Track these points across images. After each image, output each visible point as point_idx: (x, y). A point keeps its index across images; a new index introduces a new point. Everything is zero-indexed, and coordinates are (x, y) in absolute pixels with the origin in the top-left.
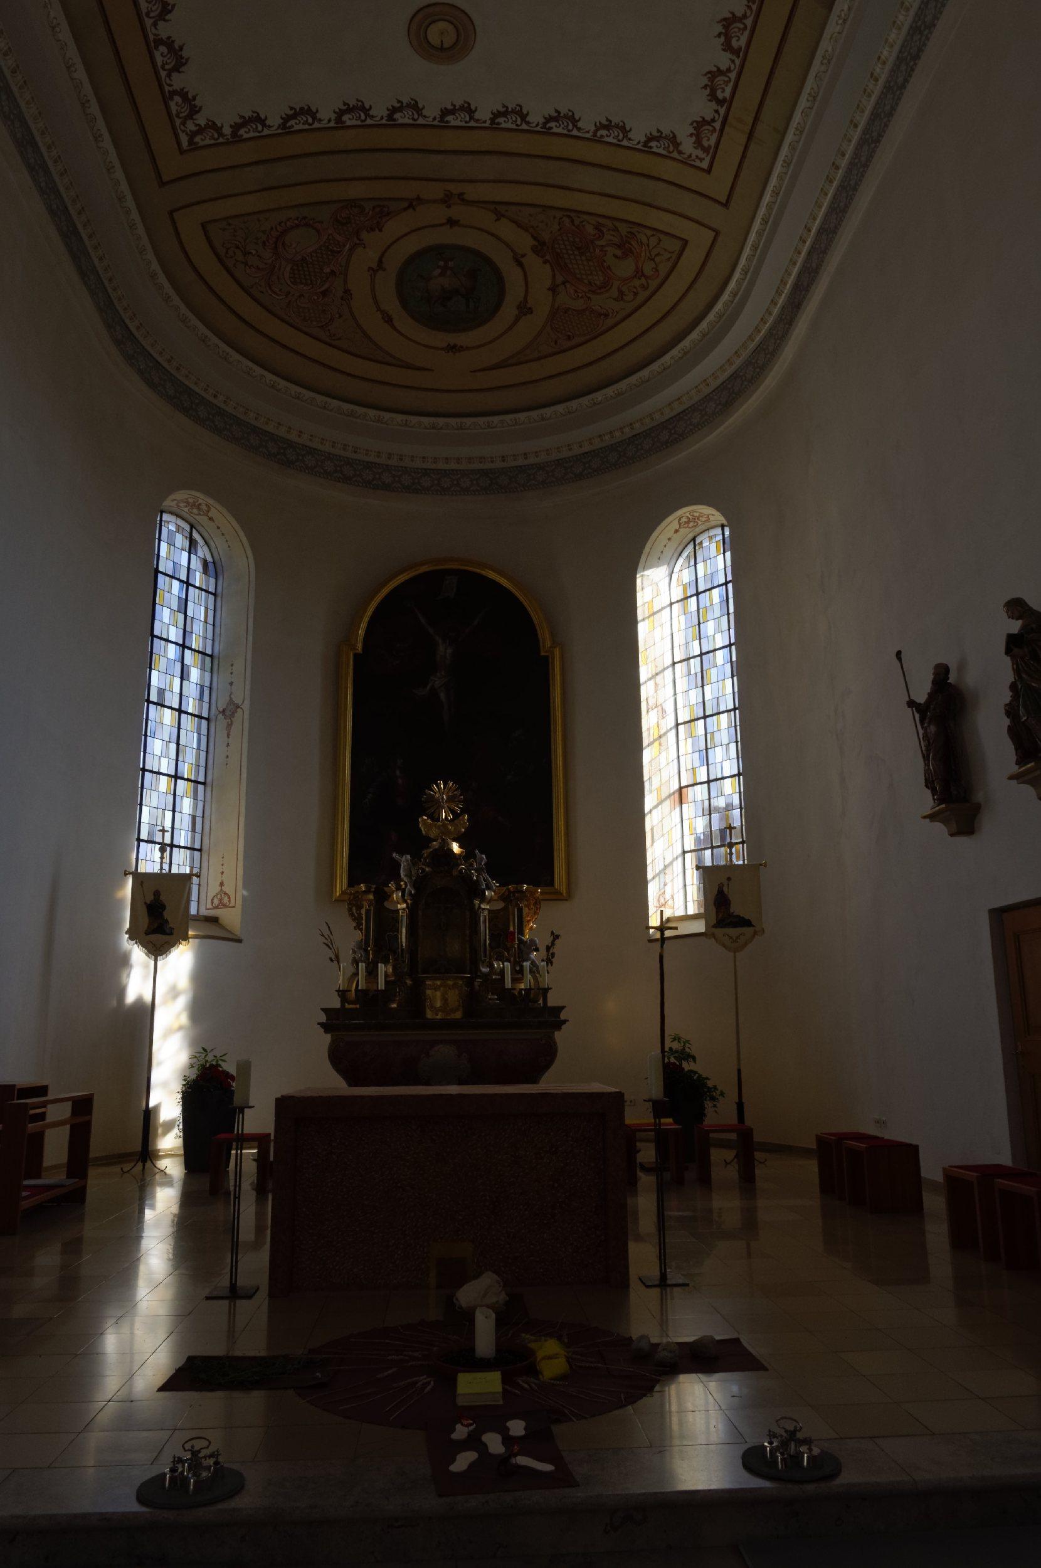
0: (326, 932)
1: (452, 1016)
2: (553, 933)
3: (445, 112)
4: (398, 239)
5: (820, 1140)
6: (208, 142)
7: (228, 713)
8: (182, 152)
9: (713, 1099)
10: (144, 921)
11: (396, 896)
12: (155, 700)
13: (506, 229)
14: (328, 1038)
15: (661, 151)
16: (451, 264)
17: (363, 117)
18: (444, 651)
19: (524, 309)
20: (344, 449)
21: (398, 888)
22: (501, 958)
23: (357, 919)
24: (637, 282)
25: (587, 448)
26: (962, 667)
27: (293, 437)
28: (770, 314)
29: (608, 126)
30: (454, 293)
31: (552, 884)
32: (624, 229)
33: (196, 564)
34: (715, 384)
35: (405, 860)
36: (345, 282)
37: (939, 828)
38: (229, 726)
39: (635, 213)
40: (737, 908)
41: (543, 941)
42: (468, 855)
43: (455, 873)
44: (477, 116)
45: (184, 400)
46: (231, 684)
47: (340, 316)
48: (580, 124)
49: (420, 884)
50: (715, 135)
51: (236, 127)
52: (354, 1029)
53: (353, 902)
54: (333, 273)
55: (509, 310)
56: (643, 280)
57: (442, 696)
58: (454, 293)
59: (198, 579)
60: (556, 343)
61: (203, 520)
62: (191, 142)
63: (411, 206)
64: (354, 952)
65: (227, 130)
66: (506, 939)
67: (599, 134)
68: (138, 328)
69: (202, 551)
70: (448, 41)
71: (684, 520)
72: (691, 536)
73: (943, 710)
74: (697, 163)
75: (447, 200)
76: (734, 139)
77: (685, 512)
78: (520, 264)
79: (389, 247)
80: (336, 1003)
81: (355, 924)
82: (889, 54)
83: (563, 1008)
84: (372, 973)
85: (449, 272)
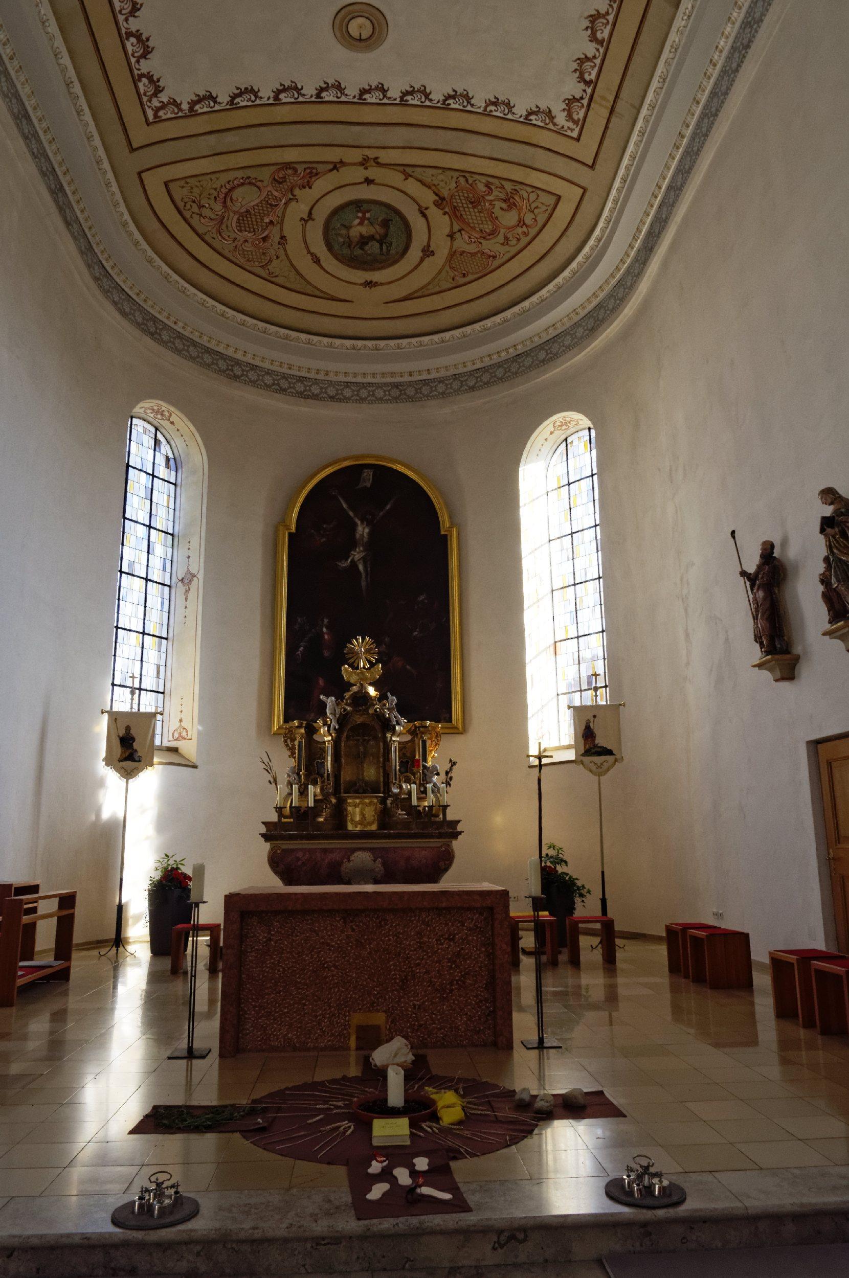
0: (266, 760)
1: (368, 828)
2: (451, 760)
3: (363, 92)
5: (669, 929)
6: (170, 116)
7: (186, 581)
9: (581, 895)
10: (118, 750)
11: (323, 730)
13: (412, 187)
14: (267, 846)
16: (368, 215)
17: (296, 96)
18: (363, 530)
19: (427, 252)
20: (281, 366)
21: (325, 724)
22: (408, 781)
23: (292, 749)
25: (478, 365)
26: (785, 543)
27: (239, 356)
28: (628, 256)
30: (371, 240)
31: (450, 720)
32: (509, 186)
33: (160, 460)
34: (582, 313)
35: (330, 701)
36: (282, 230)
37: (766, 675)
38: (187, 591)
39: (517, 174)
40: (600, 741)
41: (443, 767)
42: (382, 697)
43: (371, 711)
44: (389, 94)
45: (151, 326)
46: (189, 557)
47: (278, 258)
48: (473, 101)
49: (343, 720)
50: (583, 110)
51: (192, 104)
52: (290, 837)
53: (289, 736)
54: (271, 222)
55: (415, 253)
56: (524, 229)
57: (361, 567)
58: (371, 240)
59: (161, 471)
61: (166, 424)
62: (156, 116)
63: (335, 168)
64: (289, 776)
65: (185, 106)
66: (411, 764)
67: (488, 109)
69: (165, 449)
71: (558, 424)
72: (563, 437)
73: (769, 578)
74: (569, 133)
75: (365, 163)
76: (599, 113)
77: (558, 417)
78: (424, 216)
80: (274, 818)
81: (289, 753)
83: (459, 822)
84: (303, 792)
85: (366, 222)
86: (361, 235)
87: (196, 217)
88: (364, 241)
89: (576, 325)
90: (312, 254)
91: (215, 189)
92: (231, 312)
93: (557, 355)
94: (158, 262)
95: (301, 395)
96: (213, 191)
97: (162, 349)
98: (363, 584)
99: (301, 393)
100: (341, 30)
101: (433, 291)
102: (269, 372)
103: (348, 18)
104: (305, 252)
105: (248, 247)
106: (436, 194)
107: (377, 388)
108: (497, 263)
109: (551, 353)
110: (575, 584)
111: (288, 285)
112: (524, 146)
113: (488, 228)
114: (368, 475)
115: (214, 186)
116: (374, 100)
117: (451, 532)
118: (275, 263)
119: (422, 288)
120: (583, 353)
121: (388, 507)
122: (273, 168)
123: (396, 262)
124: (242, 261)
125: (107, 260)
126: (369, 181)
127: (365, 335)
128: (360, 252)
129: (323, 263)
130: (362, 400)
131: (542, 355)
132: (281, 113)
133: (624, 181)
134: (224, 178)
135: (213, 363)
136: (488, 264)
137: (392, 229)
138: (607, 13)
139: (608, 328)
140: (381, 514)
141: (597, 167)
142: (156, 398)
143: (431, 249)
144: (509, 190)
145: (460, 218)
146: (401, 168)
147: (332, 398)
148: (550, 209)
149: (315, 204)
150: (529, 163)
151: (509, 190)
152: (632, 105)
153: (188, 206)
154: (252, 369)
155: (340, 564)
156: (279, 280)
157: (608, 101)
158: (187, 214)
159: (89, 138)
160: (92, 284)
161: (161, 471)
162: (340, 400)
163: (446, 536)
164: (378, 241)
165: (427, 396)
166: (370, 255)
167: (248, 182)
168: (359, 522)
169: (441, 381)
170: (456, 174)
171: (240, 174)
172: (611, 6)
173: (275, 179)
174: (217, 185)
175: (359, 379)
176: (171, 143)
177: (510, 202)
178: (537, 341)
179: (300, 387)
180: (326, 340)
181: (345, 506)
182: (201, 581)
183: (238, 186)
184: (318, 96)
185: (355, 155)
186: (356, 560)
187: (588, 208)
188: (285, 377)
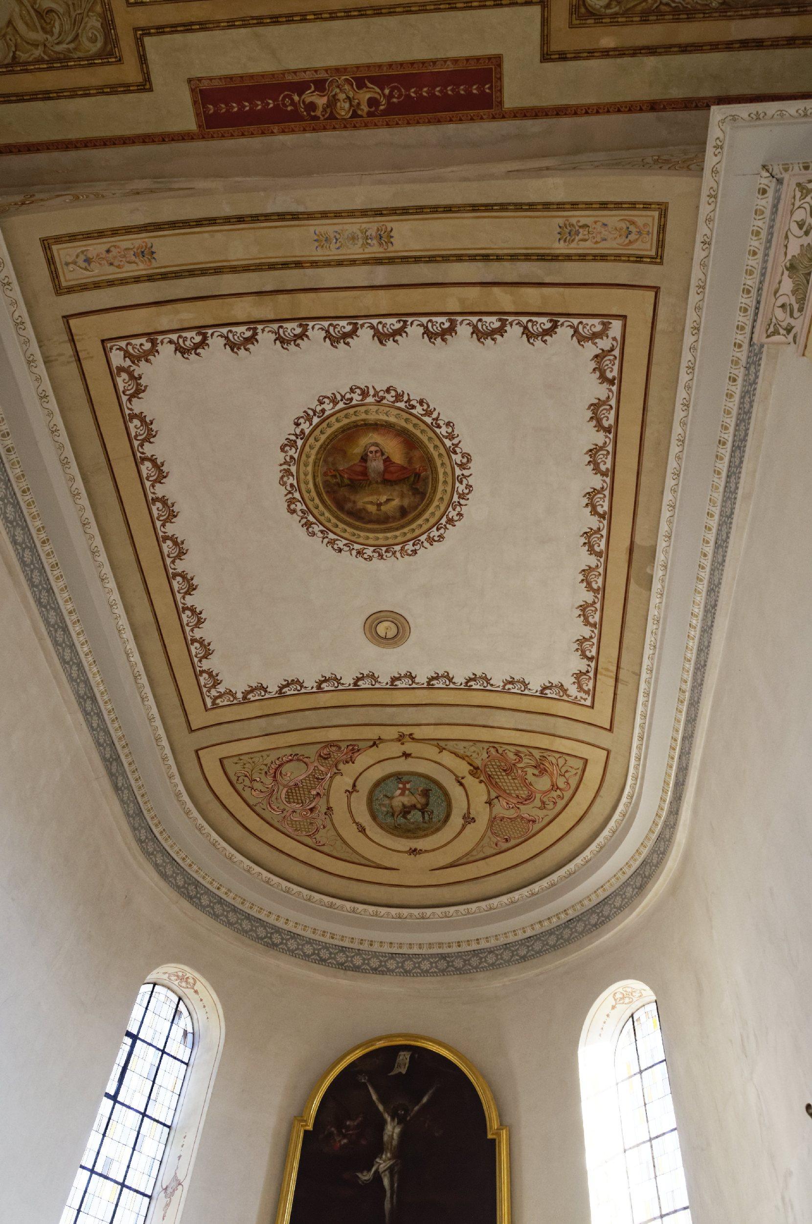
3: (394, 679)
4: (369, 768)
6: (226, 703)
7: (169, 1190)
8: (206, 710)
12: (99, 1171)
13: (447, 758)
15: (554, 696)
16: (408, 786)
17: (336, 685)
18: (392, 1130)
19: (469, 819)
20: (323, 935)
24: (554, 794)
27: (280, 924)
28: (662, 809)
29: (512, 682)
30: (413, 810)
32: (537, 754)
33: (177, 1033)
34: (629, 872)
36: (328, 802)
38: (168, 1205)
39: (544, 742)
44: (417, 680)
45: (191, 889)
47: (324, 827)
48: (491, 682)
50: (592, 682)
51: (245, 694)
54: (318, 794)
55: (456, 820)
56: (559, 792)
57: (386, 1182)
58: (413, 810)
59: (176, 1047)
60: (496, 845)
61: (190, 992)
62: (214, 703)
63: (374, 744)
65: (240, 696)
67: (507, 687)
68: (161, 833)
69: (184, 1022)
70: (392, 633)
71: (618, 996)
74: (583, 702)
75: (401, 738)
76: (606, 684)
77: (618, 987)
78: (461, 784)
79: (361, 774)
82: (699, 610)
85: (407, 792)
86: (404, 805)
87: (248, 790)
88: (406, 811)
89: (626, 884)
90: (357, 824)
91: (266, 765)
92: (276, 880)
93: (608, 918)
94: (208, 829)
95: (341, 966)
96: (263, 767)
97: (199, 913)
98: (387, 1205)
99: (342, 964)
100: (371, 632)
101: (478, 857)
102: (310, 942)
103: (376, 623)
104: (351, 821)
105: (296, 817)
106: (471, 765)
107: (424, 959)
108: (537, 827)
109: (603, 916)
110: (662, 1216)
111: (335, 854)
112: (544, 717)
113: (524, 793)
114: (404, 1058)
115: (265, 762)
116: (404, 686)
117: (499, 1135)
118: (322, 832)
119: (467, 854)
120: (635, 913)
121: (425, 1100)
122: (319, 746)
123: (438, 830)
124: (290, 830)
125: (156, 826)
126: (406, 755)
127: (412, 903)
128: (402, 820)
129: (368, 832)
130: (407, 973)
131: (594, 919)
132: (323, 700)
133: (641, 738)
134: (274, 755)
135: (251, 930)
136: (528, 829)
137: (432, 799)
138: (594, 603)
139: (653, 886)
140: (416, 1108)
141: (615, 729)
142: (181, 963)
143: (471, 816)
144: (538, 757)
145: (496, 786)
146: (435, 742)
147: (375, 970)
148: (579, 772)
149: (358, 777)
150: (552, 732)
151: (538, 757)
152: (634, 673)
153: (241, 780)
154: (292, 938)
155: (359, 1175)
156: (325, 849)
157: (612, 672)
158: (240, 787)
159: (151, 719)
160: (134, 845)
161: (176, 1047)
162: (383, 973)
163: (494, 1140)
164: (420, 810)
165: (476, 968)
166: (413, 823)
167: (296, 758)
168: (389, 1119)
169: (491, 951)
170: (486, 746)
171: (288, 751)
172: (596, 597)
173: (320, 756)
174: (268, 761)
175: (404, 950)
176: (226, 725)
177: (541, 768)
178: (588, 905)
179: (341, 958)
180: (371, 909)
181: (374, 1097)
182: (185, 1191)
183: (288, 762)
184: (355, 684)
185: (393, 732)
186: (381, 1170)
187: (615, 768)
188: (326, 947)
